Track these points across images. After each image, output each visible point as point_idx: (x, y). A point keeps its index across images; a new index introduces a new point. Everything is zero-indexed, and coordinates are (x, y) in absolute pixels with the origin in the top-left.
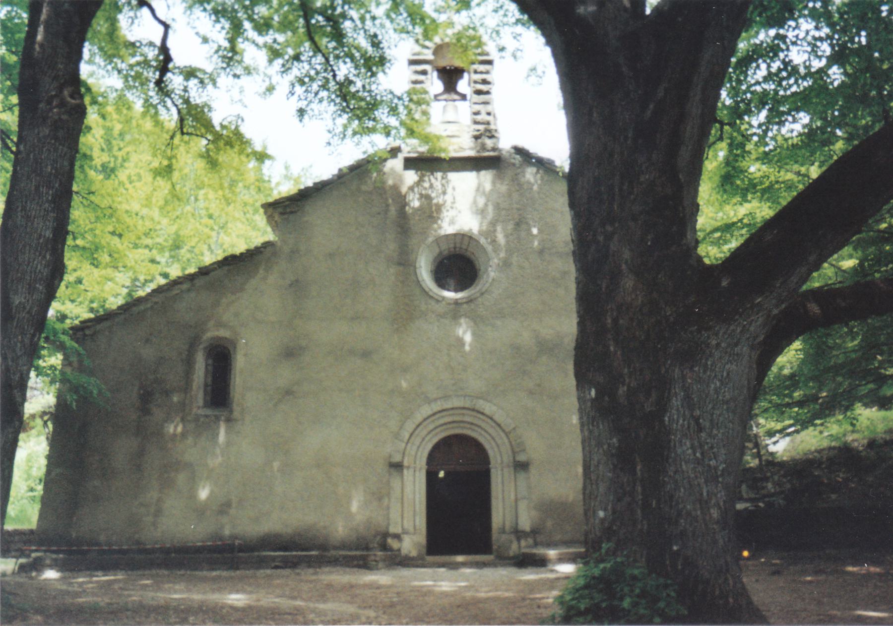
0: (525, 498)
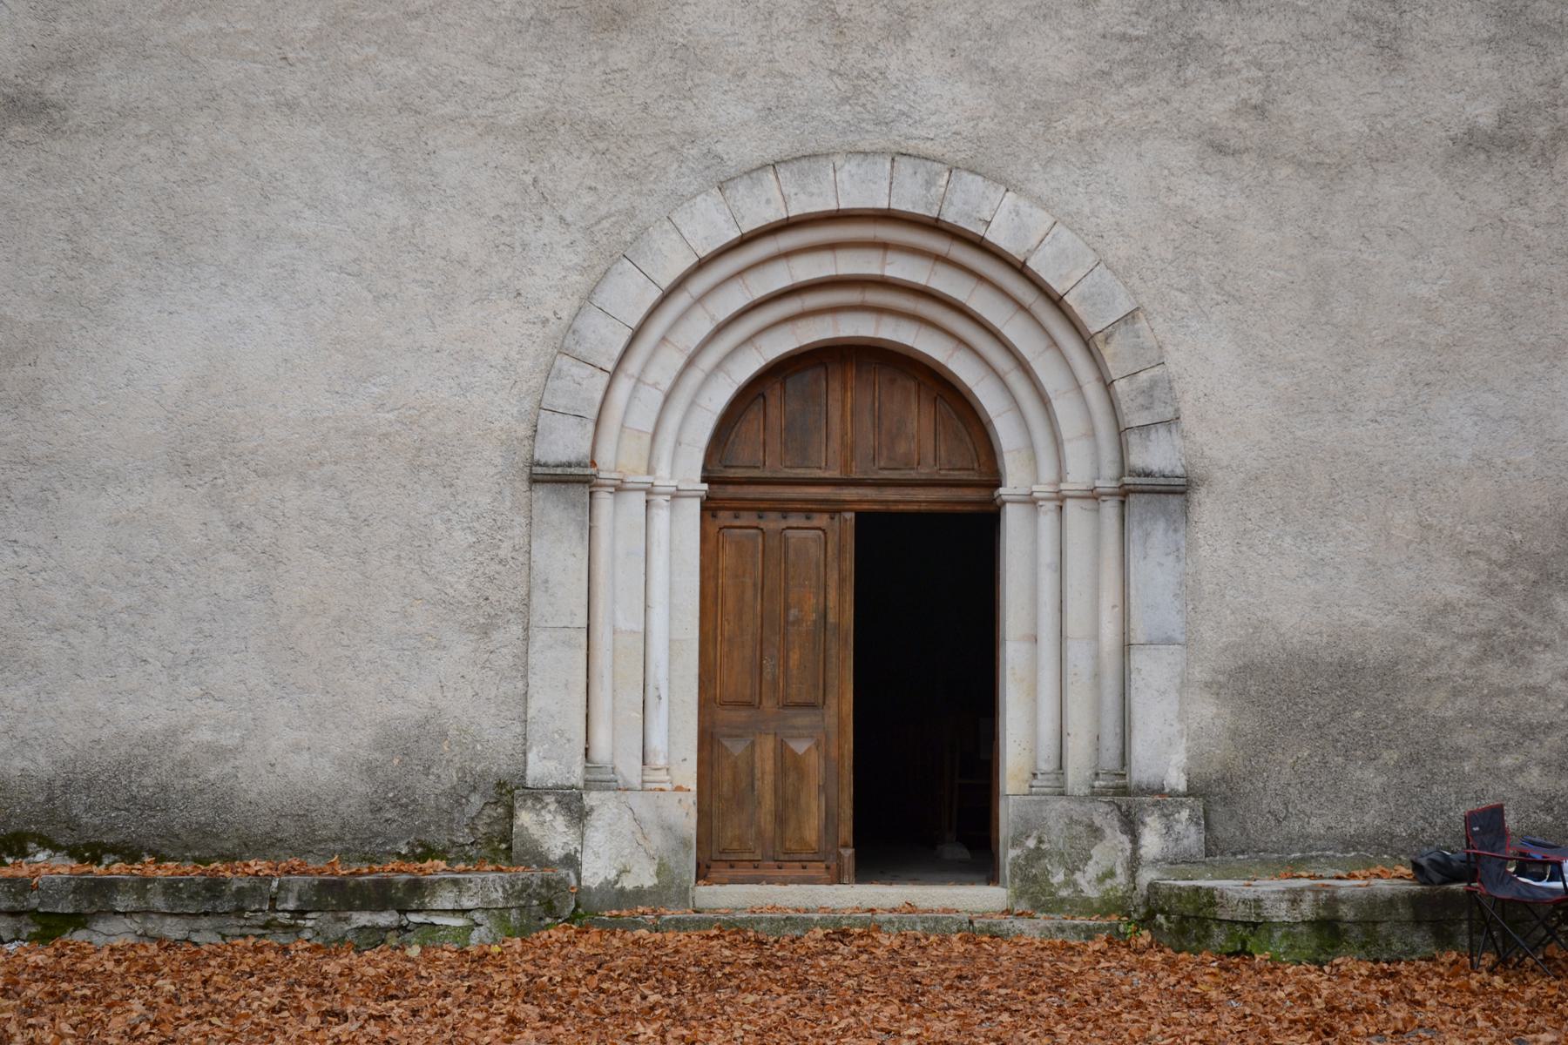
0: (1169, 641)
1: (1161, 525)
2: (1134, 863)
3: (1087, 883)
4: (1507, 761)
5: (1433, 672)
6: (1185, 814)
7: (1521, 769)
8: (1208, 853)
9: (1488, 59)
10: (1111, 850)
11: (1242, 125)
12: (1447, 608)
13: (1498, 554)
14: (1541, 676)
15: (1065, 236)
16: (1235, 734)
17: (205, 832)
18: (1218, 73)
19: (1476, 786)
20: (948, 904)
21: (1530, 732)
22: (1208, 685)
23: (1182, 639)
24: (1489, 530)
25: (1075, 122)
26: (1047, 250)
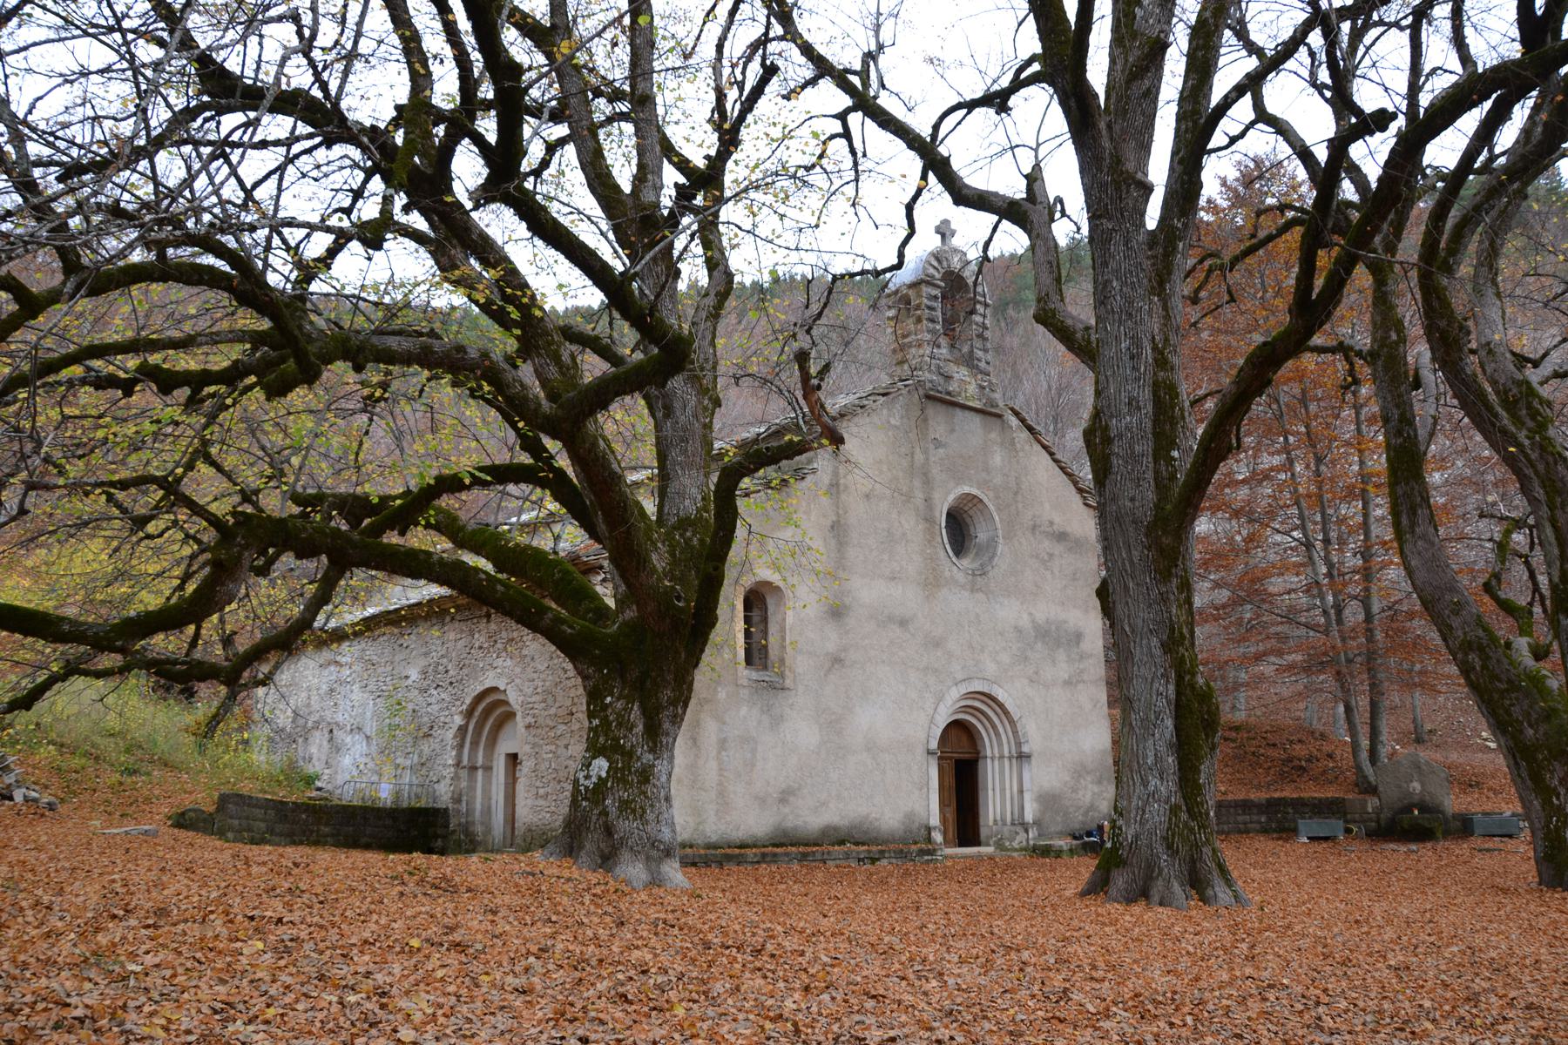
2: (1028, 840)
3: (1015, 844)
10: (1021, 837)
17: (876, 839)
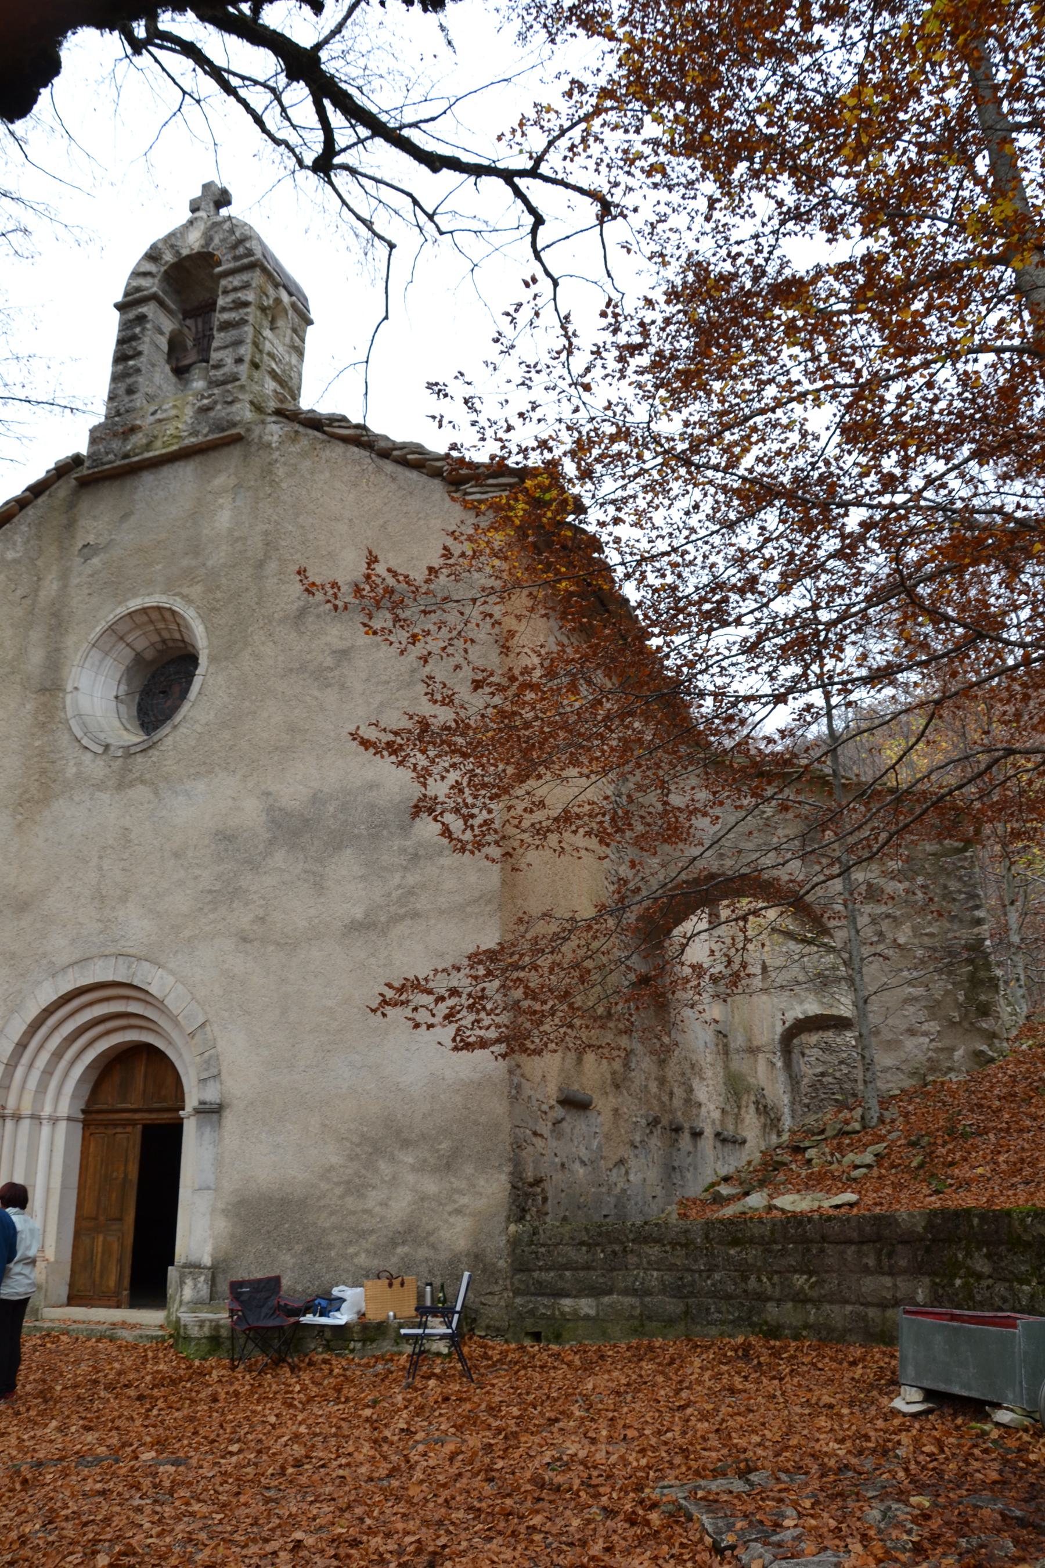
0: (208, 1188)
1: (208, 1129)
4: (351, 1250)
5: (322, 1203)
6: (202, 1278)
7: (356, 1254)
8: (211, 1299)
9: (361, 886)
11: (255, 927)
12: (331, 1168)
13: (356, 1139)
14: (370, 1204)
15: (180, 987)
16: (232, 1236)
18: (246, 904)
19: (336, 1264)
20: (139, 1321)
21: (363, 1234)
22: (223, 1211)
23: (213, 1186)
24: (352, 1126)
25: (187, 933)
26: (172, 995)
